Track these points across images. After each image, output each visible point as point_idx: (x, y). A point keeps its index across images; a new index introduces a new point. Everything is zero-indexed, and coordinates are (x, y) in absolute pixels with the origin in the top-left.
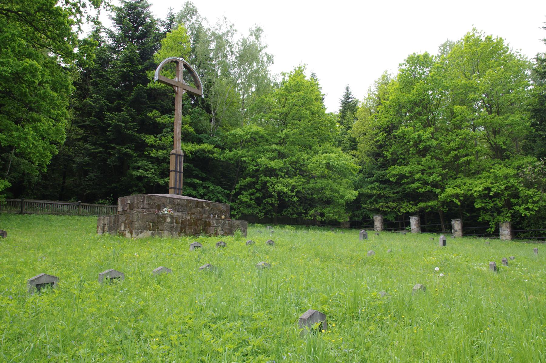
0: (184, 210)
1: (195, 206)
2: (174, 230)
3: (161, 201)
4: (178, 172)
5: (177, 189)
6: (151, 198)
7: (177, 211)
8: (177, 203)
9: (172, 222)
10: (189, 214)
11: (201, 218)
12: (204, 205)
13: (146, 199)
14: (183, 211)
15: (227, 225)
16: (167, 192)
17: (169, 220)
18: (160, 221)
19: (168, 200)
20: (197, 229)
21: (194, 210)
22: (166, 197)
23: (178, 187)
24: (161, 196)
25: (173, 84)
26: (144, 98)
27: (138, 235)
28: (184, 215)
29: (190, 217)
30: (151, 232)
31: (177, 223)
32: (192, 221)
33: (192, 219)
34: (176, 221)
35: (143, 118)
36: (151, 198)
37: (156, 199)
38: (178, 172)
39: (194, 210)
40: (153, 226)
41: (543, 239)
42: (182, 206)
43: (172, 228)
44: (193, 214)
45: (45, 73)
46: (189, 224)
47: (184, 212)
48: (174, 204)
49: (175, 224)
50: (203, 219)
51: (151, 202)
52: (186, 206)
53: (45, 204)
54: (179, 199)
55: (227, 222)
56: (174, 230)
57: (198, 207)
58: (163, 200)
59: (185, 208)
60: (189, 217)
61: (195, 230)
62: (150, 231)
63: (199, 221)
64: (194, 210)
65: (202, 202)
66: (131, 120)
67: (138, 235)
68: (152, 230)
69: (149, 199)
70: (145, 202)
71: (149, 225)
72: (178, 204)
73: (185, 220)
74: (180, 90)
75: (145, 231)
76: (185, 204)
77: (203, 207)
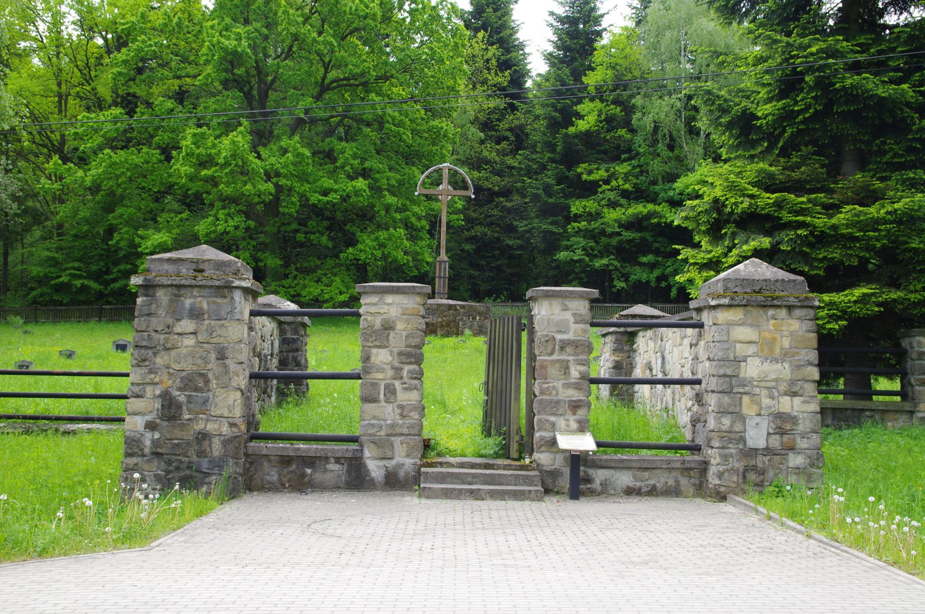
44: (445, 316)
52: (437, 310)
61: (448, 331)
65: (455, 306)
77: (456, 310)
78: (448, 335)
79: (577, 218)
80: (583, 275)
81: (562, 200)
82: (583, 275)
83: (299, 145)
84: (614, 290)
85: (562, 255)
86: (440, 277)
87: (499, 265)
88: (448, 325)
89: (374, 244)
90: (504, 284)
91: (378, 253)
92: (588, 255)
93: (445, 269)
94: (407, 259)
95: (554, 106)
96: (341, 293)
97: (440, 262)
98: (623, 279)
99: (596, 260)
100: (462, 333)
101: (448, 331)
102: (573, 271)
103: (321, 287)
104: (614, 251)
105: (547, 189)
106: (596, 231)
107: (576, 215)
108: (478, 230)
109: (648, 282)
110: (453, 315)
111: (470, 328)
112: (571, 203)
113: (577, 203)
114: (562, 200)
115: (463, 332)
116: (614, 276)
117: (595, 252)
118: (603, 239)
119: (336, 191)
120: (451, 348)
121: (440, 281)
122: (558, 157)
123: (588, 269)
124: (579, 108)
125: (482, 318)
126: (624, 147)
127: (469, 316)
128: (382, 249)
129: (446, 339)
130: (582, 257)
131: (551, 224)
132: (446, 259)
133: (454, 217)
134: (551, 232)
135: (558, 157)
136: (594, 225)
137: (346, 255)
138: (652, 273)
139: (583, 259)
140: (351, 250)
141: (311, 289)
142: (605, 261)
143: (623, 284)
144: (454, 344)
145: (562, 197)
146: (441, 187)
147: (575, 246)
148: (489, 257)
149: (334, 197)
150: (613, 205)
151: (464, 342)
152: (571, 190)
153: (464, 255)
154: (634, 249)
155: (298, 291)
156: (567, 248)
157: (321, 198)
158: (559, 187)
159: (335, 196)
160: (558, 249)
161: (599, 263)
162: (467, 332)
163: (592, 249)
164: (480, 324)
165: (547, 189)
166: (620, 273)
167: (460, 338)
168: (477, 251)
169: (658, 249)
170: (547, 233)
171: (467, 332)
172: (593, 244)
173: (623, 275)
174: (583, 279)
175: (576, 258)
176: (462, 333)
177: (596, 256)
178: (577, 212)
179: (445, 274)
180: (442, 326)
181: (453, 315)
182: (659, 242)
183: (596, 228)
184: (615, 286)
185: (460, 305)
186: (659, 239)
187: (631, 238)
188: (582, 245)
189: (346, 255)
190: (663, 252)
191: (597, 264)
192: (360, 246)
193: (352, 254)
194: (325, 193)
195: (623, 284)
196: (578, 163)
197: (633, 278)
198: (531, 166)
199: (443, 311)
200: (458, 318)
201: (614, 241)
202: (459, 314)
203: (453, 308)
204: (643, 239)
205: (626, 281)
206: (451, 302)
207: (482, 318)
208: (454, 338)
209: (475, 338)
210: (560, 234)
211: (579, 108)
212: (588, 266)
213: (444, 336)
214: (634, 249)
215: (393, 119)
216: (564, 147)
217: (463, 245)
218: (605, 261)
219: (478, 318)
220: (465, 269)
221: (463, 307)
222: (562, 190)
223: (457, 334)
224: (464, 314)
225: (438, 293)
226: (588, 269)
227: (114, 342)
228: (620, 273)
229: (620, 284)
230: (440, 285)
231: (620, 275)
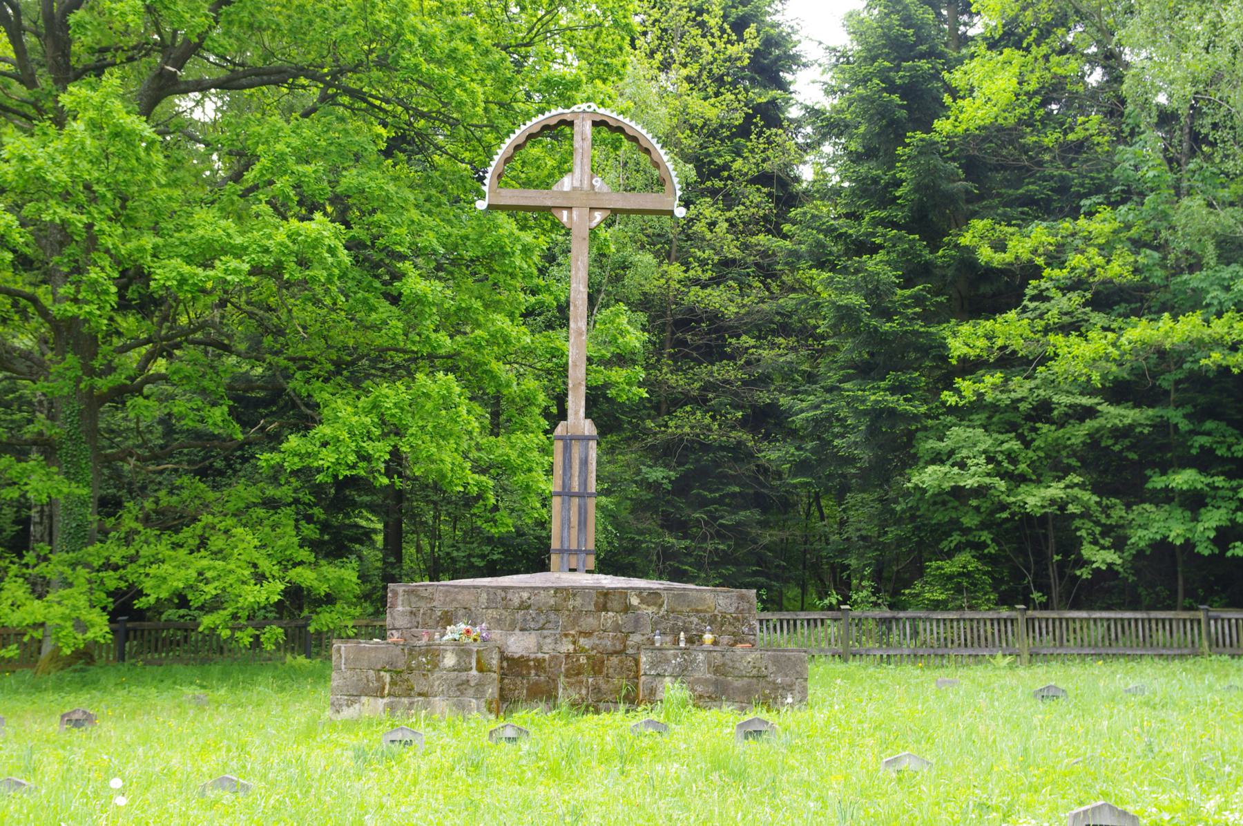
0: (550, 625)
1: (592, 608)
2: (471, 691)
3: (454, 600)
4: (573, 495)
5: (570, 552)
6: (418, 596)
7: (522, 630)
8: (516, 602)
9: (461, 668)
10: (566, 635)
11: (619, 647)
12: (635, 601)
13: (400, 598)
14: (542, 629)
15: (703, 667)
16: (543, 566)
17: (450, 660)
18: (419, 665)
19: (484, 596)
20: (604, 687)
21: (591, 620)
22: (475, 587)
23: (574, 546)
24: (455, 587)
25: (549, 203)
26: (952, 177)
27: (338, 712)
28: (548, 640)
29: (571, 648)
30: (386, 700)
31: (480, 670)
32: (583, 660)
33: (583, 650)
34: (478, 661)
35: (952, 257)
36: (418, 596)
37: (436, 596)
38: (573, 495)
39: (589, 622)
40: (393, 683)
41: (1240, 656)
42: (539, 611)
43: (462, 686)
44: (588, 634)
45: (753, 137)
46: (567, 670)
47: (545, 632)
48: (506, 608)
49: (474, 672)
50: (630, 651)
51: (418, 609)
52: (556, 609)
53: (1150, 620)
54: (524, 589)
55: (701, 657)
56: (471, 691)
57: (605, 608)
58: (464, 597)
59: (552, 616)
60: (566, 646)
61: (597, 690)
62: (383, 697)
63: (615, 660)
64: (589, 622)
65: (623, 593)
66: (898, 277)
67: (338, 712)
68: (389, 695)
69: (414, 599)
70: (400, 608)
71: (379, 679)
72: (524, 606)
73: (553, 658)
74: (580, 216)
75: (364, 699)
76: (552, 602)
77: (627, 608)
78: (596, 703)
79: (970, 367)
80: (986, 536)
81: (919, 326)
82: (986, 536)
83: (118, 104)
84: (1084, 573)
85: (929, 477)
86: (566, 493)
87: (739, 524)
88: (597, 666)
89: (368, 420)
90: (755, 573)
91: (380, 450)
92: (1003, 475)
93: (584, 462)
94: (478, 484)
95: (883, 75)
96: (260, 578)
97: (568, 441)
98: (1107, 542)
99: (1023, 488)
100: (652, 697)
101: (597, 690)
102: (955, 525)
103: (203, 561)
104: (1074, 462)
105: (875, 293)
106: (1023, 406)
107: (964, 360)
108: (684, 423)
109: (1189, 545)
110: (617, 628)
111: (681, 673)
112: (947, 333)
113: (966, 328)
114: (919, 326)
115: (652, 692)
116: (1083, 533)
117: (1022, 467)
118: (1045, 428)
119: (239, 252)
120: (606, 760)
121: (566, 509)
122: (899, 215)
123: (1005, 515)
124: (957, 78)
125: (725, 639)
126: (1082, 185)
127: (675, 632)
128: (393, 440)
129: (591, 719)
130: (988, 480)
131: (893, 390)
132: (588, 428)
133: (618, 375)
134: (892, 413)
135: (899, 215)
136: (1020, 387)
137: (276, 458)
138: (1195, 519)
139: (989, 487)
140: (293, 442)
141: (166, 568)
142: (1056, 490)
143: (1111, 557)
144: (621, 739)
145: (918, 316)
146: (567, 183)
147: (964, 453)
148: (714, 501)
149: (232, 269)
150: (1072, 327)
151: (661, 728)
152: (942, 299)
153: (647, 495)
154: (1133, 456)
155: (131, 579)
156: (937, 459)
157: (186, 269)
158: (908, 292)
159: (234, 263)
160: (913, 461)
161: (1034, 498)
162: (672, 690)
163: (1012, 458)
164: (719, 660)
165: (875, 293)
166: (1097, 523)
167: (642, 715)
168: (681, 487)
169: (1207, 452)
170: (880, 415)
171: (672, 690)
172: (1015, 445)
173: (1107, 531)
174: (984, 545)
175: (970, 482)
176: (652, 697)
177: (1022, 479)
178: (965, 350)
179: (584, 483)
180: (575, 672)
181: (617, 628)
182: (1209, 434)
183: (1022, 399)
184: (1082, 562)
185: (639, 591)
186: (1209, 425)
187: (1128, 421)
188: (982, 447)
189: (276, 458)
190: (1223, 460)
191: (1031, 501)
192: (324, 430)
193: (296, 454)
194: (206, 255)
195: (1111, 557)
196: (962, 221)
197: (1140, 538)
198: (824, 246)
199: (575, 620)
200: (635, 638)
201: (1078, 433)
202: (637, 625)
203: (615, 604)
204: (1162, 427)
205: (1119, 545)
206: (608, 581)
207: (725, 639)
208: (620, 715)
209: (703, 714)
210: (916, 418)
211: (957, 78)
212: (1004, 507)
213: (581, 707)
214: (1133, 456)
215: (427, 43)
216: (916, 189)
217: (644, 469)
218: (1056, 490)
219: (708, 638)
220: (650, 532)
221: (652, 597)
222: (918, 300)
223: (632, 700)
224: (655, 625)
225: (561, 551)
226: (1005, 515)
227: (740, 726)
228: (1097, 523)
229: (1102, 557)
230: (566, 522)
231: (1098, 530)
